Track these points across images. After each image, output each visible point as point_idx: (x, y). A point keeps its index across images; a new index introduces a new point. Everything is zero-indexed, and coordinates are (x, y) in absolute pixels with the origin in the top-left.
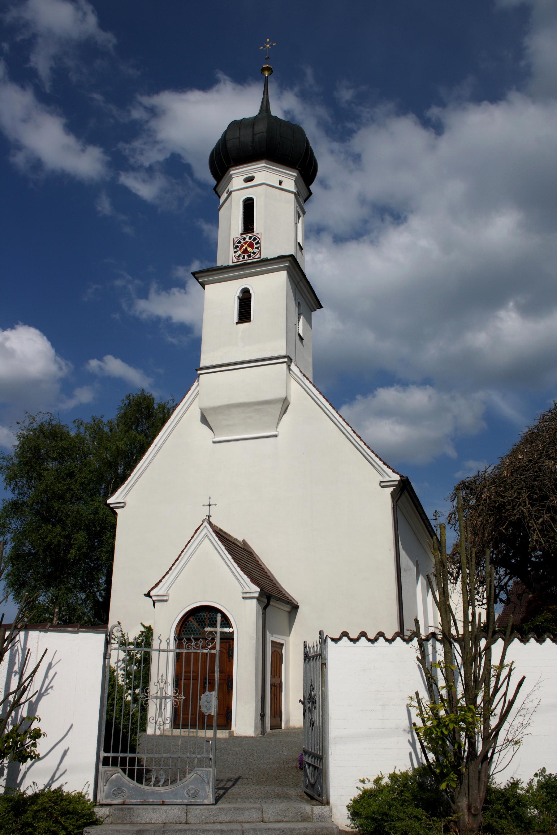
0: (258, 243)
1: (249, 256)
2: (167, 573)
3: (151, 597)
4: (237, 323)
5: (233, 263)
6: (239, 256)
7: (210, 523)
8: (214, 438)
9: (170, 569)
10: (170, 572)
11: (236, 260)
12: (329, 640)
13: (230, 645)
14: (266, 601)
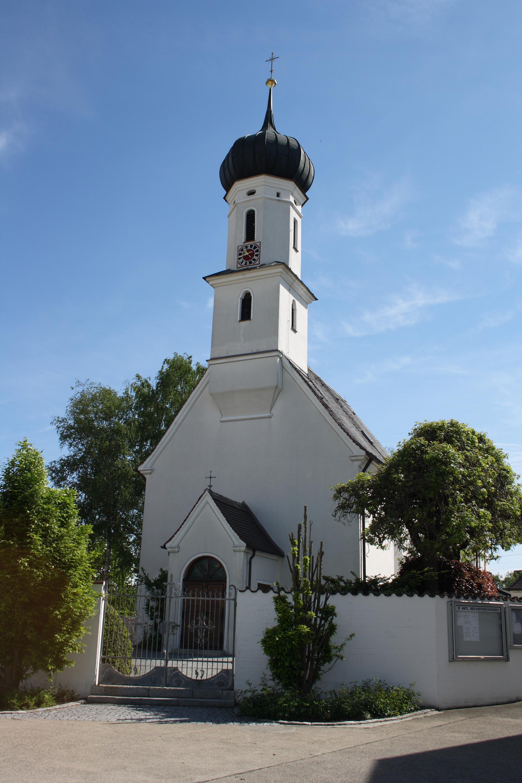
0: (257, 251)
1: (250, 263)
2: (178, 530)
3: (166, 549)
4: (239, 321)
5: (237, 268)
6: (242, 263)
7: (211, 492)
8: (222, 418)
9: (181, 527)
10: (180, 530)
11: (239, 266)
12: (238, 591)
13: (224, 586)
14: (252, 552)
